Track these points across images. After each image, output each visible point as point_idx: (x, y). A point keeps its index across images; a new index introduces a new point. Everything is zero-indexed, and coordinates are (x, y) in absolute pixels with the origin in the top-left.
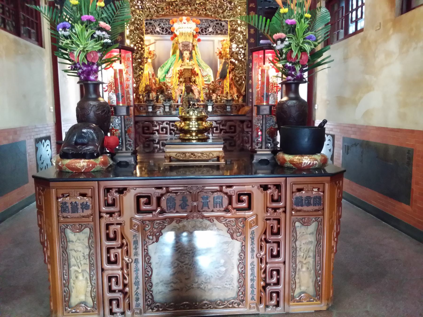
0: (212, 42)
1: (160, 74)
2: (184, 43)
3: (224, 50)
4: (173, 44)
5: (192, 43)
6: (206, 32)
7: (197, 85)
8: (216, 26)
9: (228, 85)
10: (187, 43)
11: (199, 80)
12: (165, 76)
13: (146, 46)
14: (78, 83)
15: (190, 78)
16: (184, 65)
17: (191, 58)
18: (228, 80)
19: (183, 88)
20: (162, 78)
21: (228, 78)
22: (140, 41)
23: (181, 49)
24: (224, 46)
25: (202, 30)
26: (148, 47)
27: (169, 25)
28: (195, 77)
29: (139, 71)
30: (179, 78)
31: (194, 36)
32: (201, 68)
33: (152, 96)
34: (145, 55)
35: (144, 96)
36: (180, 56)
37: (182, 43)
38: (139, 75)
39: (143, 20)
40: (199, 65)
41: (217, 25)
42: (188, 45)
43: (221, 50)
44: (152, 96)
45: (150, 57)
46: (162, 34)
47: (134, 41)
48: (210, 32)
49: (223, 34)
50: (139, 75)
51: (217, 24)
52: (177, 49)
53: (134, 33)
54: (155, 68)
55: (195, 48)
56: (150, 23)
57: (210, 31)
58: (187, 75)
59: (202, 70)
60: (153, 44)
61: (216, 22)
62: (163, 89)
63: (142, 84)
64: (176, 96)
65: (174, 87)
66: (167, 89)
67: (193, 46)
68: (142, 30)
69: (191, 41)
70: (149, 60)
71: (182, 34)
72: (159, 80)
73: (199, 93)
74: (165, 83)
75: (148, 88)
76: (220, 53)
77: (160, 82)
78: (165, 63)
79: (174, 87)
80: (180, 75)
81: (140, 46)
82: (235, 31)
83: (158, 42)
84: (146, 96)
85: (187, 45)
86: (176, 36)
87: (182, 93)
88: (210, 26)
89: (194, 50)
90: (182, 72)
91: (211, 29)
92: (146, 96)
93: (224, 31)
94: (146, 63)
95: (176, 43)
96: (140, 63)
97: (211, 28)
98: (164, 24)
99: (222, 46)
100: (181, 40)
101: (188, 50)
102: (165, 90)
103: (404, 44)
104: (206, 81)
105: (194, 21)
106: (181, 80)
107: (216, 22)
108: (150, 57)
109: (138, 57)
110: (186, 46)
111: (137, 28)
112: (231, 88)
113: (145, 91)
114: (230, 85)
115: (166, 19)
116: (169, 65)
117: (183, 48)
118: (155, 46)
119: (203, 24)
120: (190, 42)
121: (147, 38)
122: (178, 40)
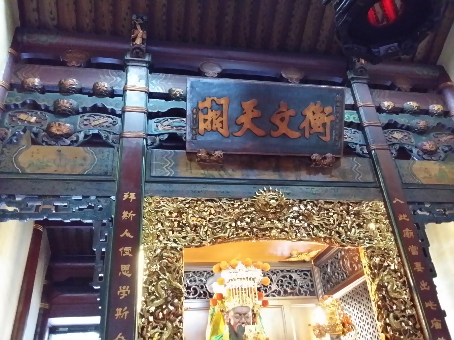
0: (280, 309)
2: (240, 310)
5: (253, 311)
6: (266, 291)
10: (244, 310)
14: (99, 337)
22: (173, 298)
23: (232, 323)
37: (234, 309)
41: (284, 280)
48: (274, 292)
49: (297, 295)
51: (284, 277)
57: (273, 289)
61: (281, 274)
67: (254, 315)
68: (178, 273)
69: (251, 308)
81: (172, 308)
85: (245, 314)
93: (297, 288)
97: (275, 284)
100: (231, 304)
107: (281, 274)
115: (194, 272)
117: (237, 320)
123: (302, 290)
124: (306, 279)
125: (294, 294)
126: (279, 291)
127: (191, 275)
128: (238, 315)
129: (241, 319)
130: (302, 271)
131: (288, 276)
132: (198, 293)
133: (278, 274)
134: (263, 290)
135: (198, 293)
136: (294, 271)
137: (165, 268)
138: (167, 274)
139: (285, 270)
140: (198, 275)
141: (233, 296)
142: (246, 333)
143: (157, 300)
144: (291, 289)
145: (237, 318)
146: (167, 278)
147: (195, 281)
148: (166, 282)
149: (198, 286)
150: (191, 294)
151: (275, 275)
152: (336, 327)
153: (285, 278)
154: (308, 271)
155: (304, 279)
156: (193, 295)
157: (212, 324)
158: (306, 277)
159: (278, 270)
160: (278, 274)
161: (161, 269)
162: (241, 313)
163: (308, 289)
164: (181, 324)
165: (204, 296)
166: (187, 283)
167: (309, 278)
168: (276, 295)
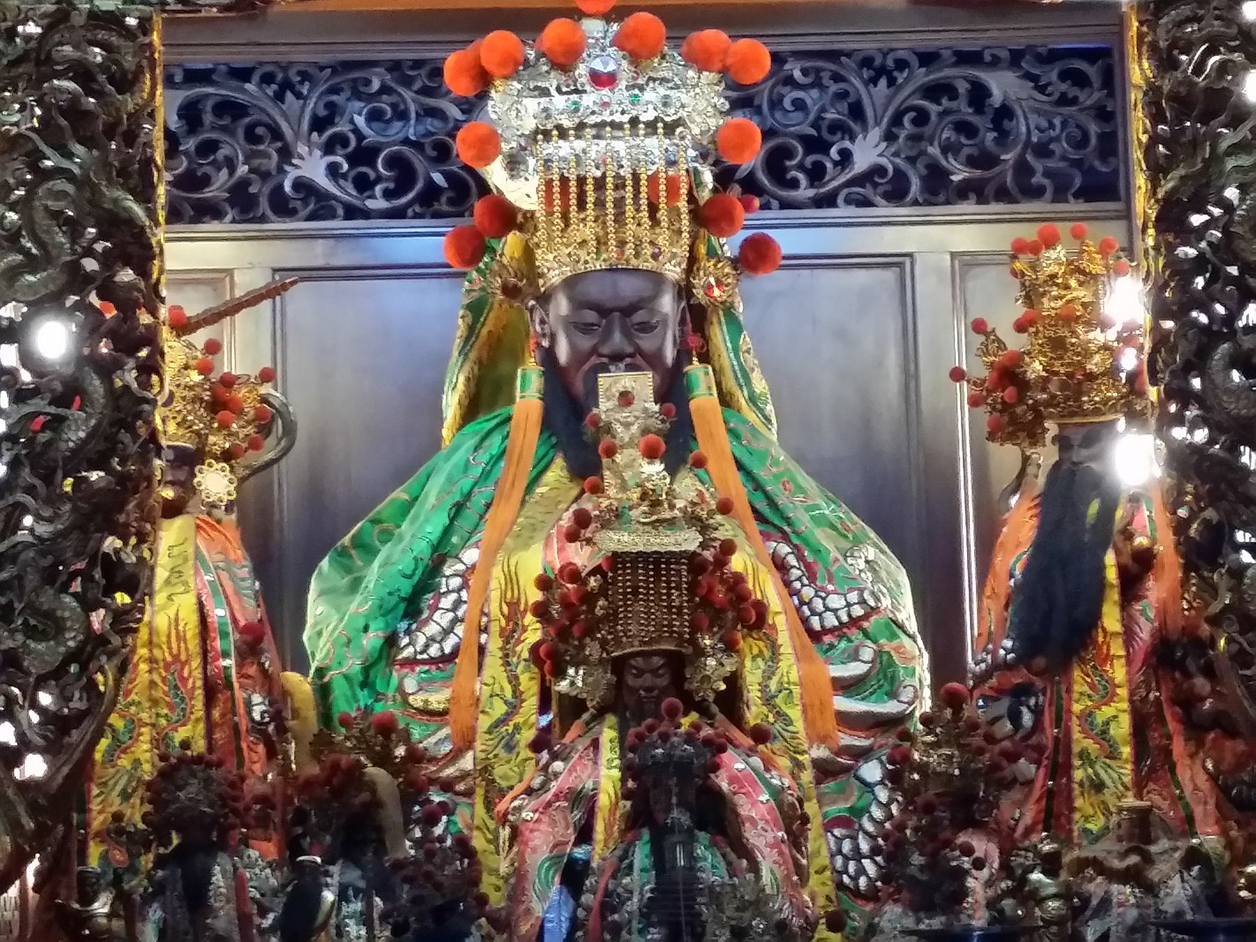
0: (888, 276)
1: (333, 621)
2: (595, 291)
3: (1058, 345)
4: (476, 309)
5: (684, 291)
6: (816, 174)
7: (760, 735)
8: (922, 118)
9: (1118, 718)
10: (629, 288)
11: (778, 674)
12: (391, 641)
13: (183, 327)
15: (679, 664)
16: (615, 518)
17: (676, 443)
18: (1119, 672)
19: (607, 778)
20: (354, 665)
21: (1117, 648)
22: (108, 261)
23: (563, 353)
24: (1049, 305)
25: (776, 162)
26: (200, 338)
27: (431, 124)
28: (730, 647)
29: (88, 606)
30: (551, 661)
31: (707, 218)
32: (784, 549)
33: (239, 885)
34: (170, 428)
35: (137, 885)
36: (547, 423)
37: (571, 283)
38: (93, 646)
39: (145, 25)
40: (771, 520)
41: (933, 109)
42: (645, 303)
43: (1016, 343)
44: (239, 885)
45: (217, 442)
46: (352, 212)
47: (32, 264)
49: (1003, 195)
50: (93, 646)
51: (934, 91)
52: (517, 358)
53: (44, 175)
54: (281, 557)
55: (719, 335)
56: (230, 109)
57: (861, 163)
58: (637, 630)
59: (801, 567)
60: (253, 299)
61: (922, 76)
62: (375, 804)
63: (119, 746)
64: (519, 874)
65: (485, 770)
66: (412, 791)
67: (697, 317)
68: (130, 137)
69: (673, 271)
70: (215, 482)
71: (570, 193)
72: (323, 691)
73: (793, 823)
74: (387, 728)
75: (190, 792)
76: (1009, 374)
77: (325, 715)
78: (383, 508)
79: (485, 770)
80: (563, 634)
82: (1206, 118)
83: (301, 297)
84: (158, 891)
85: (628, 310)
86: (507, 217)
87: (585, 834)
88: (857, 111)
89: (705, 358)
90: (589, 598)
91: (867, 151)
92: (158, 891)
94: (173, 510)
95: (511, 292)
96: (101, 513)
97: (875, 134)
98: (374, 116)
99: (1031, 295)
101: (635, 360)
102: (392, 813)
103: (1156, 580)
104: (846, 686)
105: (700, 61)
106: (572, 681)
107: (922, 76)
108: (217, 442)
109: (76, 434)
110: (612, 319)
111: (74, 112)
112: (1152, 760)
113: (158, 827)
114: (1144, 722)
115: (395, 67)
116: (434, 529)
117: (586, 343)
118: (279, 337)
119: (790, 95)
120: (656, 278)
121: (191, 255)
122: (528, 253)
123: (1038, 165)
124: (1074, 101)
125: (990, 190)
126: (898, 172)
127: (376, 85)
128: (591, 316)
129: (607, 335)
130: (1053, 56)
131: (962, 87)
132: (420, 185)
133: (901, 77)
134: (801, 167)
135: (420, 185)
136: (1004, 54)
137: (63, 122)
138: (79, 149)
139: (946, 54)
140: (417, 86)
141: (565, 217)
142: (605, 407)
143: (33, 273)
144: (971, 162)
145: (586, 328)
146: (76, 171)
147: (402, 115)
148: (70, 188)
149: (417, 146)
150: (378, 189)
151: (883, 82)
152: (1079, 393)
153: (945, 101)
154: (1091, 55)
155: (1064, 100)
156: (388, 194)
157: (473, 355)
158: (1074, 92)
159: (901, 54)
160: (901, 77)
161: (47, 128)
162: (609, 305)
163: (1077, 164)
164: (155, 378)
165: (451, 202)
166: (356, 131)
167: (1090, 98)
168: (878, 200)
